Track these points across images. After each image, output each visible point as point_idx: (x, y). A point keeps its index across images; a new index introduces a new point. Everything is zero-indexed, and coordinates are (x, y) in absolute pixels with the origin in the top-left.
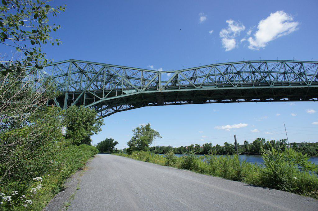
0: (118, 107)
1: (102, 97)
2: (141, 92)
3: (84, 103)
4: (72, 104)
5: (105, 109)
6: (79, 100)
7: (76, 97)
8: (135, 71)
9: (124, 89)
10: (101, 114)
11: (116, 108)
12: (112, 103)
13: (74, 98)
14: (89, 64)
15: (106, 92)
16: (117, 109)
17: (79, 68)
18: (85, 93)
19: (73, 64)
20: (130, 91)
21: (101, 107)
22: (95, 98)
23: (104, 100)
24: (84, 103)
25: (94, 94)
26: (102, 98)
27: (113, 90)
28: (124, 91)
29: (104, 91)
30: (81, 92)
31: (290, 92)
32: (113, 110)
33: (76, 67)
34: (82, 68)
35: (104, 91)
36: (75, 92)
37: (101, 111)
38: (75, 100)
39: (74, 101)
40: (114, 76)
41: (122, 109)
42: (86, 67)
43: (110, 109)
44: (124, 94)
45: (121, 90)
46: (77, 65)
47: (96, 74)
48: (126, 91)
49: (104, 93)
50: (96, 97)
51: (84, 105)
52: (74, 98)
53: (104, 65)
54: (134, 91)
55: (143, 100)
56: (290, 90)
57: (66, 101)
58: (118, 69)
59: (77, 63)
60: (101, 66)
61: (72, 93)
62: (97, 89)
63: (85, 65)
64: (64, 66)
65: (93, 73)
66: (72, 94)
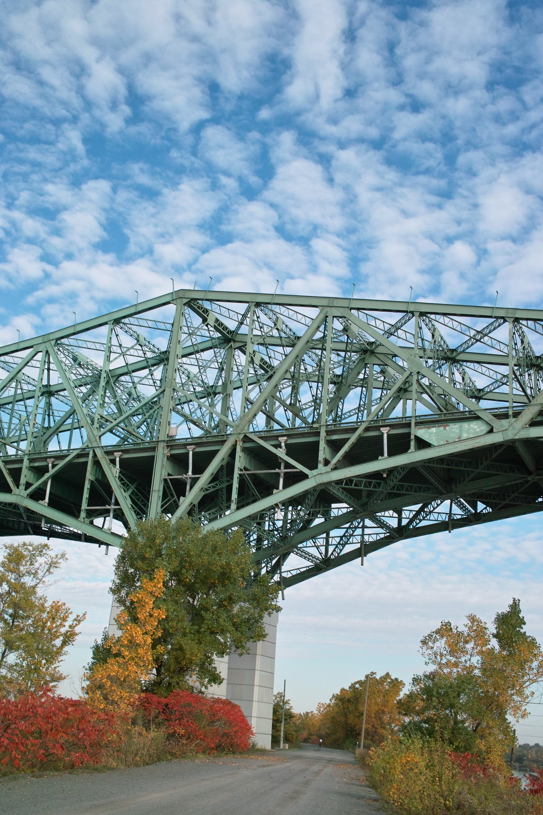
0: (409, 511)
1: (315, 467)
2: (510, 436)
3: (234, 495)
4: (182, 498)
5: (338, 522)
6: (215, 478)
7: (199, 469)
8: (481, 324)
9: (423, 422)
10: (323, 549)
11: (400, 513)
12: (370, 494)
13: (190, 473)
14: (258, 305)
15: (335, 437)
16: (404, 522)
17: (219, 326)
18: (238, 449)
19: (188, 311)
20: (454, 429)
21: (326, 514)
22: (283, 470)
23: (325, 479)
24: (234, 495)
25: (281, 453)
26: (315, 472)
27: (367, 429)
28: (422, 433)
29: (323, 434)
30: (223, 442)
31: (445, 466)
32: (382, 525)
33: (205, 320)
34: (232, 325)
35: (323, 434)
36: (197, 442)
37: (325, 529)
38: (194, 481)
39: (191, 488)
40: (380, 350)
41: (424, 523)
42: (244, 316)
43: (368, 522)
44: (422, 444)
45: (409, 425)
46: (206, 311)
47: (293, 346)
48: (434, 430)
49: (322, 445)
50: (288, 466)
51: (233, 506)
52: (190, 473)
53: (325, 302)
54: (476, 427)
55: (530, 473)
56: (442, 466)
57: (157, 486)
58: (393, 318)
59: (207, 305)
60: (313, 313)
61: (185, 445)
62: (298, 422)
63: (241, 308)
64: (65, 352)
65: (278, 342)
66: (43, 464)
